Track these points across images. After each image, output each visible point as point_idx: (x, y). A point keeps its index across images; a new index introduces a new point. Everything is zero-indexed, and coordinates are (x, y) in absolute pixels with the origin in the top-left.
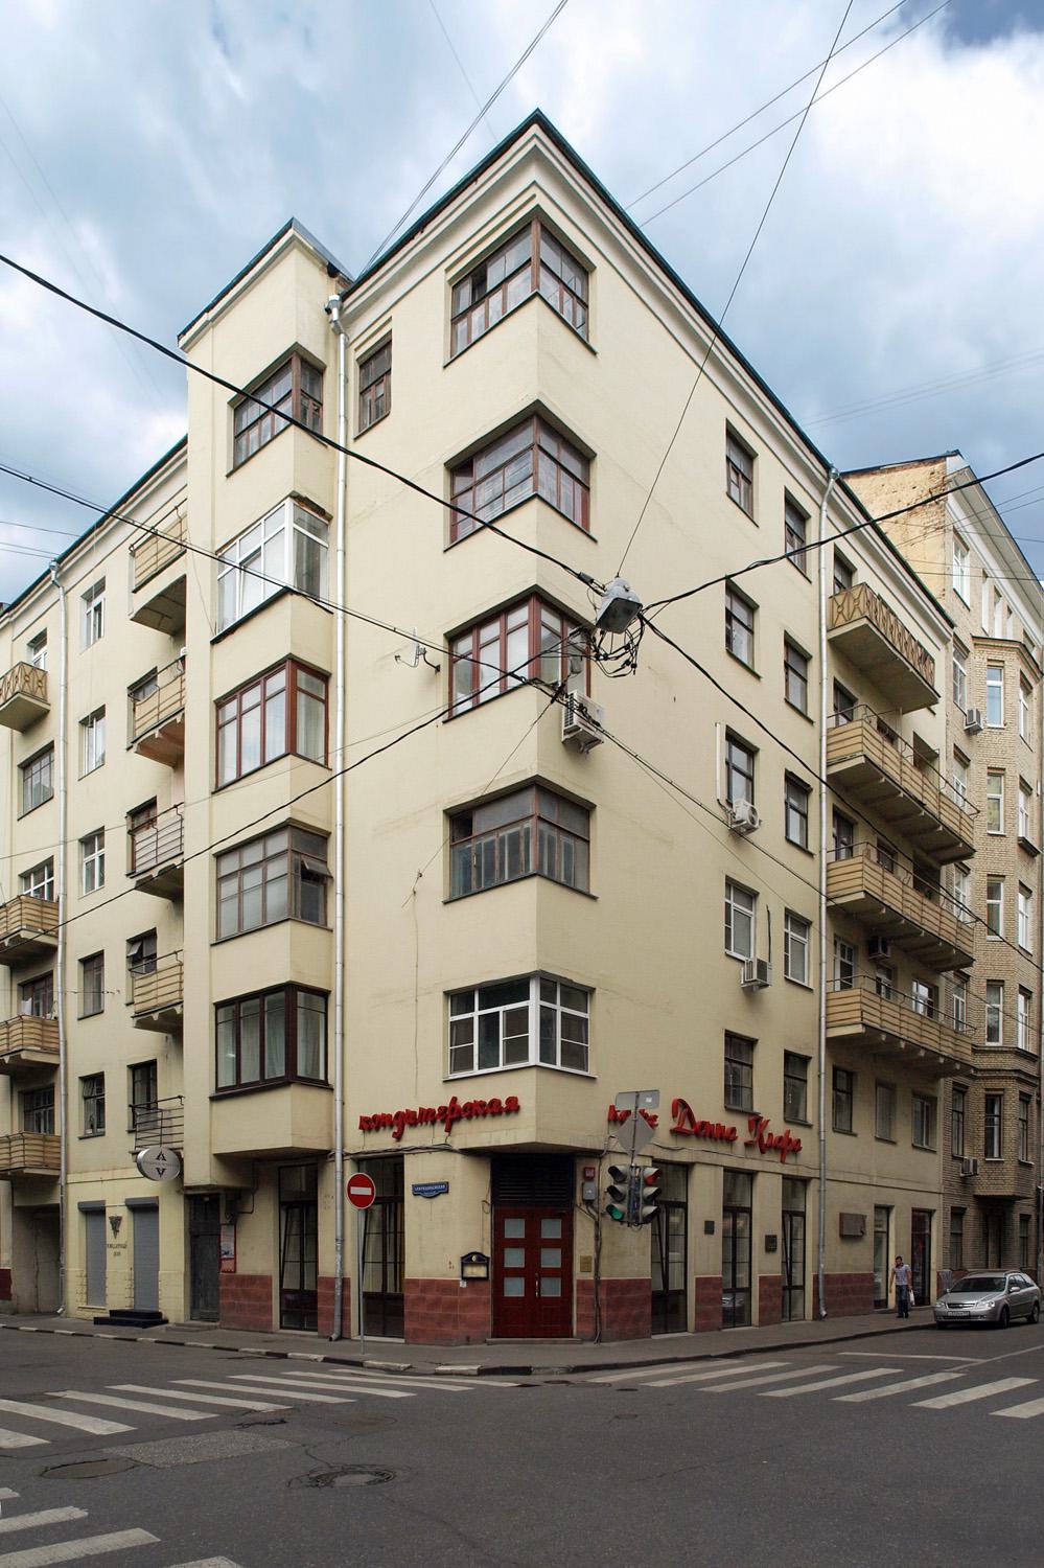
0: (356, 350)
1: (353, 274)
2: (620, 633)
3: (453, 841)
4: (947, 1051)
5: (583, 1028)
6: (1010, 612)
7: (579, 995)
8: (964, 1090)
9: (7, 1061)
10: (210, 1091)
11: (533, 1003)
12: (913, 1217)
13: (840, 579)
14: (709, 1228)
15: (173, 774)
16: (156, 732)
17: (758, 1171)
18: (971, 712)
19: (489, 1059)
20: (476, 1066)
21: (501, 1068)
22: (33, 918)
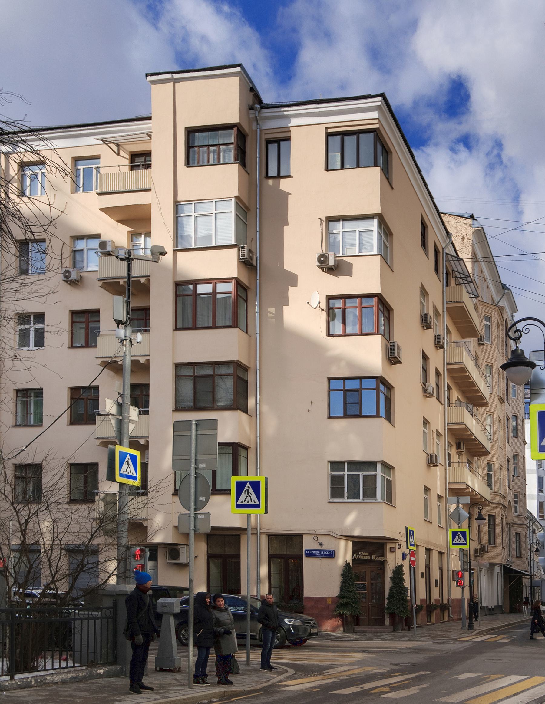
0: (319, 670)
1: (420, 152)
5: (399, 674)
6: (308, 303)
8: (41, 391)
9: (142, 282)
10: (382, 422)
13: (459, 397)
15: (115, 375)
20: (346, 498)
21: (360, 500)
22: (84, 649)
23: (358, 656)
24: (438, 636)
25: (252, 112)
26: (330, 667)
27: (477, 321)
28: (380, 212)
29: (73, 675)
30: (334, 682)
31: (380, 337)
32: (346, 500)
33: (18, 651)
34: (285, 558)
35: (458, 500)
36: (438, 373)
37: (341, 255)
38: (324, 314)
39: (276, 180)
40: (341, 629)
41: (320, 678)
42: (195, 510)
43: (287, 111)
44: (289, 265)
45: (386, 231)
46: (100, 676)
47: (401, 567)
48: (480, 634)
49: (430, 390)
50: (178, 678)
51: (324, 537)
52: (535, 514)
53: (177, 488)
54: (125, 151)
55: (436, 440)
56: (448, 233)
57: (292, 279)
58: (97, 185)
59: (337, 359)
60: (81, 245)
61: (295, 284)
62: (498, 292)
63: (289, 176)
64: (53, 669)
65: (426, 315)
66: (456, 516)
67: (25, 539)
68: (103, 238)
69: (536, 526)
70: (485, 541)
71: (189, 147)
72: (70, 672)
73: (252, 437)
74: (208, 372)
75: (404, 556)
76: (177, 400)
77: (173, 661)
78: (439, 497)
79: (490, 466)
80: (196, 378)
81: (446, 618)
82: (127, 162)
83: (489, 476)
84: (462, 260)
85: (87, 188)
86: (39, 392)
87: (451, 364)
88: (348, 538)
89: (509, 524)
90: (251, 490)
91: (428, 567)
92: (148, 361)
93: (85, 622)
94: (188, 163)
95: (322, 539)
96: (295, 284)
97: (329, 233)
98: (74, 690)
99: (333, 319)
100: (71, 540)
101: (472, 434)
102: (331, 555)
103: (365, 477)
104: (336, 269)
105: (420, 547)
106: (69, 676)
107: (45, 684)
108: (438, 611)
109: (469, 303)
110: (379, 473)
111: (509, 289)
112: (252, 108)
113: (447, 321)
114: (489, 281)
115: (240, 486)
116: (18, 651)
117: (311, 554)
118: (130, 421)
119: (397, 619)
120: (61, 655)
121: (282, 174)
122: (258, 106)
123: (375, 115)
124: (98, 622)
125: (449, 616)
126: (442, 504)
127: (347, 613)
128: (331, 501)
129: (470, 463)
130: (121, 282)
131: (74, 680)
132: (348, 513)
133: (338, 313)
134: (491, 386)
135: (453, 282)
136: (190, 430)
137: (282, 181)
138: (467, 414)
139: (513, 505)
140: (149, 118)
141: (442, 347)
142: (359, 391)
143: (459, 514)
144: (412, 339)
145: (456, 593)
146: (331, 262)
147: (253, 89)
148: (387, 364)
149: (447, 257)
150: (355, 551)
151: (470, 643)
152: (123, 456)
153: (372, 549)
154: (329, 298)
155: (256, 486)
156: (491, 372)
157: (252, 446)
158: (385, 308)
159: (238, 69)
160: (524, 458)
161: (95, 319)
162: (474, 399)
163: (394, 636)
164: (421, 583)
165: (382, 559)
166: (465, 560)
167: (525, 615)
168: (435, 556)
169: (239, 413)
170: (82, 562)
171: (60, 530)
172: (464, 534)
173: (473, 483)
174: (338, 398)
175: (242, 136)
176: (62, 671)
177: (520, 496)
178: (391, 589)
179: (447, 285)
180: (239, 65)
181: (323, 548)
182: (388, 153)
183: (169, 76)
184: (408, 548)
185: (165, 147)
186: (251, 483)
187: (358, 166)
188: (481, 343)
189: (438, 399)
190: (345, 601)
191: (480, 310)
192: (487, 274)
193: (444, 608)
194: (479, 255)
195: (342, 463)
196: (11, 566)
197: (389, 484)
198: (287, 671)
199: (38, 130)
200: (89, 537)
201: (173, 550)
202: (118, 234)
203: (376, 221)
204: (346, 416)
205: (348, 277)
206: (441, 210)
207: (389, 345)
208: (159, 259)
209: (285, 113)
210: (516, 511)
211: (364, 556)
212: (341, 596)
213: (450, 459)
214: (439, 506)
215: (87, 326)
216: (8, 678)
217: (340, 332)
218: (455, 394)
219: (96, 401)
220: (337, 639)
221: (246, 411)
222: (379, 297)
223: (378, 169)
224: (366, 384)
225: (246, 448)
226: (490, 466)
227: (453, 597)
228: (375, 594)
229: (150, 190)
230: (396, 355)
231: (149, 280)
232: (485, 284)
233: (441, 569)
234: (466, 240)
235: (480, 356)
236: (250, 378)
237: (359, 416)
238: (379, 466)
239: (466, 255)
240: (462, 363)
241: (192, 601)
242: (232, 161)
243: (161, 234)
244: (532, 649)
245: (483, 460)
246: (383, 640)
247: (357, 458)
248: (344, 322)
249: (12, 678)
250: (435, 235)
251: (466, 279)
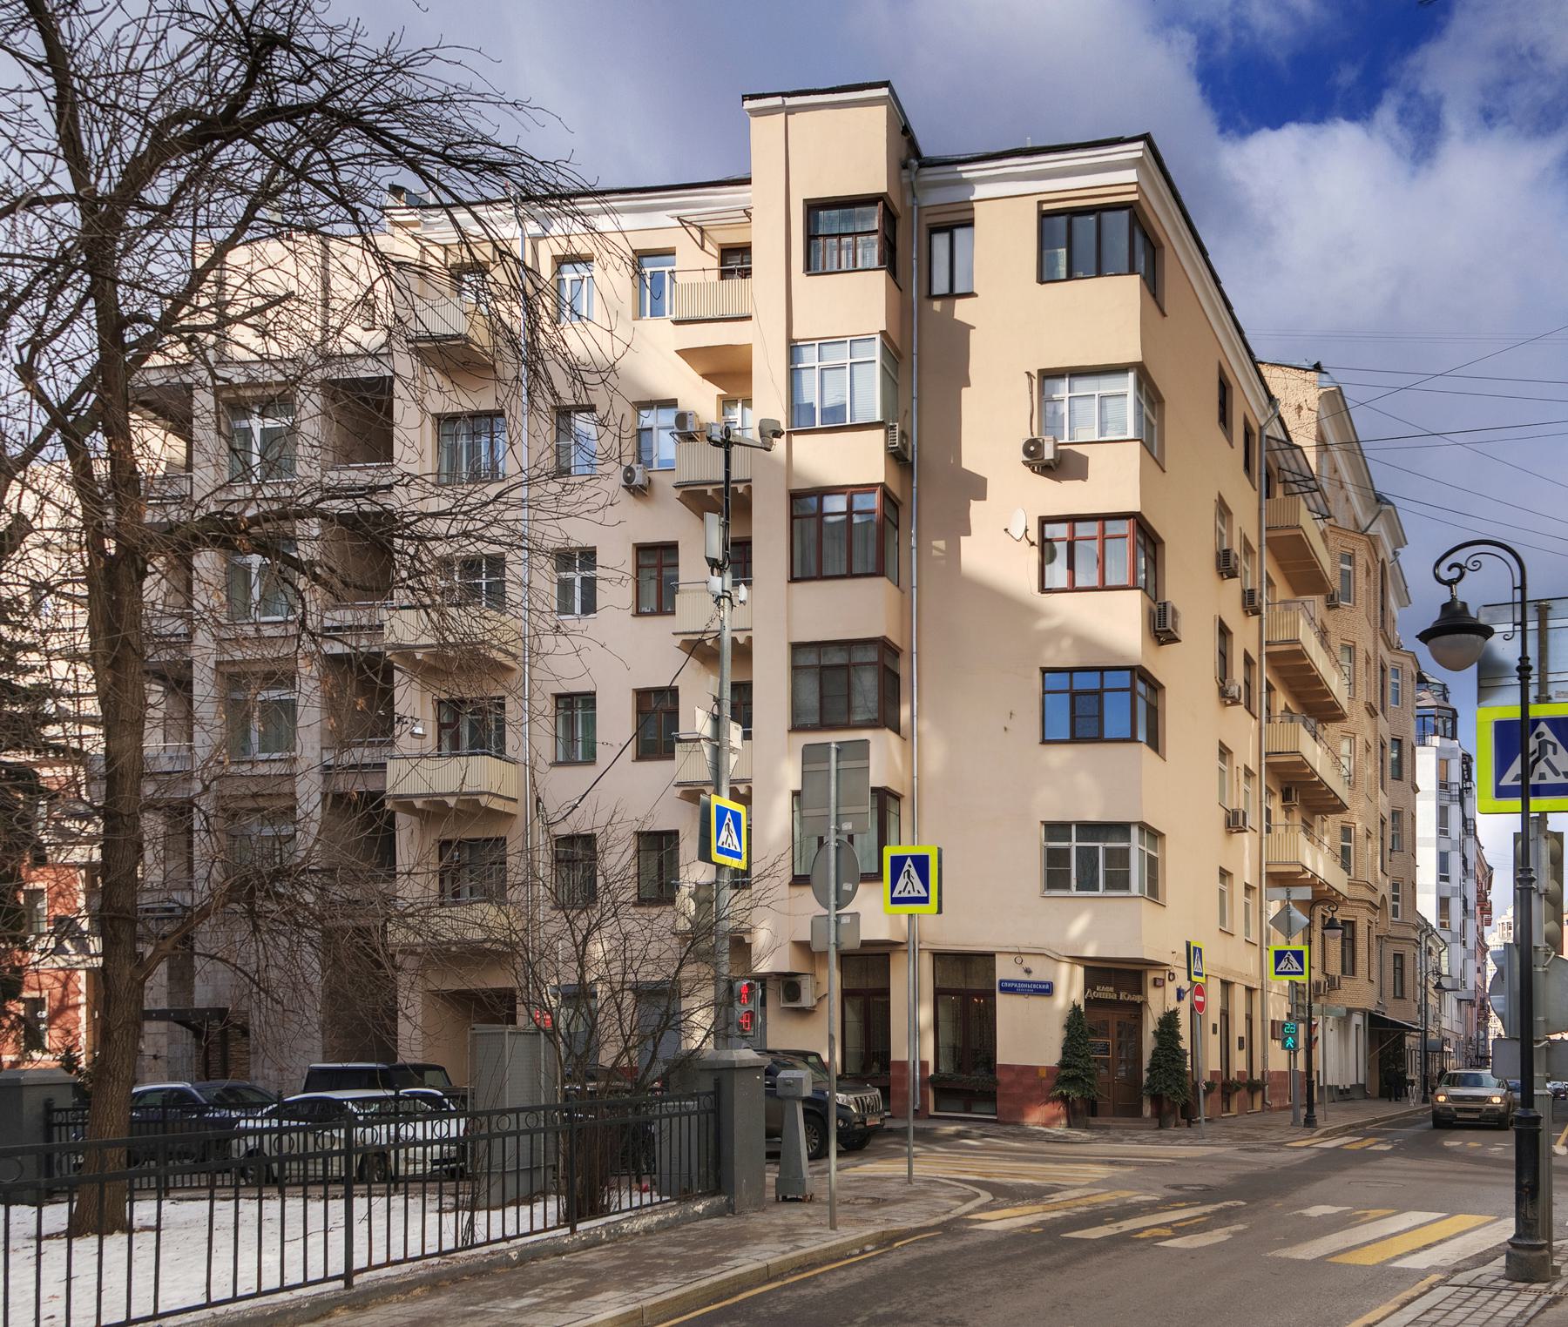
0: (1036, 1194)
2: (21, 379)
3: (344, 746)
4: (300, 450)
21: (1100, 893)
22: (675, 1169)
23: (1102, 1172)
24: (1245, 1137)
25: (905, 173)
26: (1054, 1189)
27: (1327, 562)
28: (1139, 359)
29: (661, 1217)
30: (1066, 1217)
31: (1138, 593)
32: (1074, 892)
33: (578, 1180)
34: (965, 995)
35: (1288, 893)
36: (1248, 661)
37: (1066, 440)
38: (1035, 551)
39: (947, 302)
40: (1064, 1122)
41: (1039, 1208)
42: (838, 907)
43: (969, 172)
44: (972, 458)
45: (1151, 395)
46: (698, 1217)
47: (1175, 1012)
48: (1327, 1135)
49: (1234, 691)
50: (811, 1212)
52: (1432, 919)
54: (712, 240)
55: (1243, 785)
56: (1271, 398)
57: (976, 487)
58: (676, 306)
59: (1058, 633)
60: (648, 419)
61: (981, 495)
62: (1367, 509)
63: (971, 295)
64: (631, 1209)
65: (1227, 553)
66: (1284, 923)
67: (583, 972)
68: (682, 407)
69: (1434, 942)
70: (1335, 968)
71: (811, 237)
72: (654, 1213)
73: (907, 778)
74: (837, 658)
75: (1180, 994)
76: (795, 712)
77: (802, 1183)
78: (1248, 888)
79: (1346, 832)
80: (823, 669)
81: (1258, 1105)
82: (715, 263)
83: (1345, 851)
84: (1300, 447)
85: (657, 312)
86: (589, 699)
87: (1275, 644)
88: (1077, 960)
91: (1225, 1015)
92: (750, 639)
93: (676, 1120)
94: (809, 268)
95: (1029, 962)
96: (981, 495)
97: (1044, 398)
98: (663, 1244)
99: (1052, 560)
100: (649, 974)
101: (1314, 773)
102: (1045, 990)
103: (1107, 850)
104: (1059, 465)
106: (655, 1218)
107: (621, 1236)
108: (1244, 1092)
109: (1312, 529)
110: (1136, 845)
111: (1389, 503)
112: (905, 166)
113: (1268, 565)
114: (1350, 487)
115: (898, 862)
116: (578, 1180)
117: (1011, 988)
118: (733, 750)
119: (1166, 1106)
120: (639, 1181)
121: (958, 290)
122: (914, 162)
123: (1131, 175)
124: (694, 1118)
125: (1264, 1102)
126: (1253, 901)
127: (1074, 1094)
128: (1047, 893)
129: (1308, 827)
130: (710, 490)
131: (664, 1226)
132: (1076, 915)
133: (1061, 548)
134: (1352, 684)
135: (1279, 492)
136: (828, 760)
137: (959, 303)
138: (1305, 736)
139: (1390, 903)
140: (747, 181)
141: (1257, 612)
142: (1099, 694)
143: (1289, 919)
144: (1200, 596)
145: (1277, 1059)
146: (1049, 454)
147: (906, 130)
148: (1151, 645)
149: (1268, 444)
150: (1089, 984)
151: (1307, 1152)
152: (722, 812)
153: (1117, 981)
154: (1044, 521)
155: (921, 863)
156: (1352, 659)
157: (907, 794)
158: (1148, 539)
159: (884, 92)
160: (1414, 817)
161: (672, 561)
162: (1317, 707)
163: (1160, 1136)
164: (1213, 1044)
165: (1138, 999)
166: (1301, 1001)
167: (1412, 1102)
168: (1239, 994)
169: (888, 734)
170: (667, 1011)
171: (635, 954)
172: (1298, 955)
173: (1315, 862)
174: (1061, 705)
175: (890, 218)
176: (644, 1211)
177: (1404, 888)
178: (1155, 1054)
179: (1268, 497)
180: (886, 84)
181: (1032, 978)
182: (1154, 249)
183: (777, 101)
184: (1189, 979)
185: (772, 237)
186: (913, 858)
187: (1099, 274)
188: (1332, 604)
189: (1248, 708)
190: (1071, 1072)
191: (1331, 544)
192: (1346, 474)
193: (1253, 1087)
194: (1331, 438)
195: (1067, 825)
196: (562, 1025)
197: (1153, 865)
198: (978, 1195)
199: (603, 193)
200: (677, 964)
201: (789, 984)
202: (702, 400)
203: (1131, 375)
204: (1074, 739)
205: (1080, 482)
206: (1258, 358)
207: (1155, 608)
208: (771, 443)
209: (965, 175)
210: (1395, 915)
211: (1106, 992)
212: (1063, 1065)
213: (1268, 819)
214: (1247, 904)
215: (660, 573)
216: (567, 1230)
217: (1064, 584)
218: (1281, 700)
219: (673, 715)
220: (1058, 1140)
221: (897, 730)
222: (1137, 519)
223: (1137, 278)
224: (1112, 680)
225: (898, 797)
226: (1346, 832)
227: (1271, 1069)
228: (1126, 1063)
229: (749, 318)
230: (1169, 626)
231: (749, 488)
232: (1342, 494)
233: (1249, 1018)
234: (1304, 412)
235: (1331, 627)
236: (903, 671)
237: (1099, 739)
238: (1135, 831)
239: (1305, 438)
240: (1297, 642)
242: (876, 265)
243: (768, 402)
245: (1333, 822)
246: (1140, 1142)
247: (1092, 817)
248: (1071, 566)
249: (573, 1231)
250: (1246, 402)
251: (1307, 483)
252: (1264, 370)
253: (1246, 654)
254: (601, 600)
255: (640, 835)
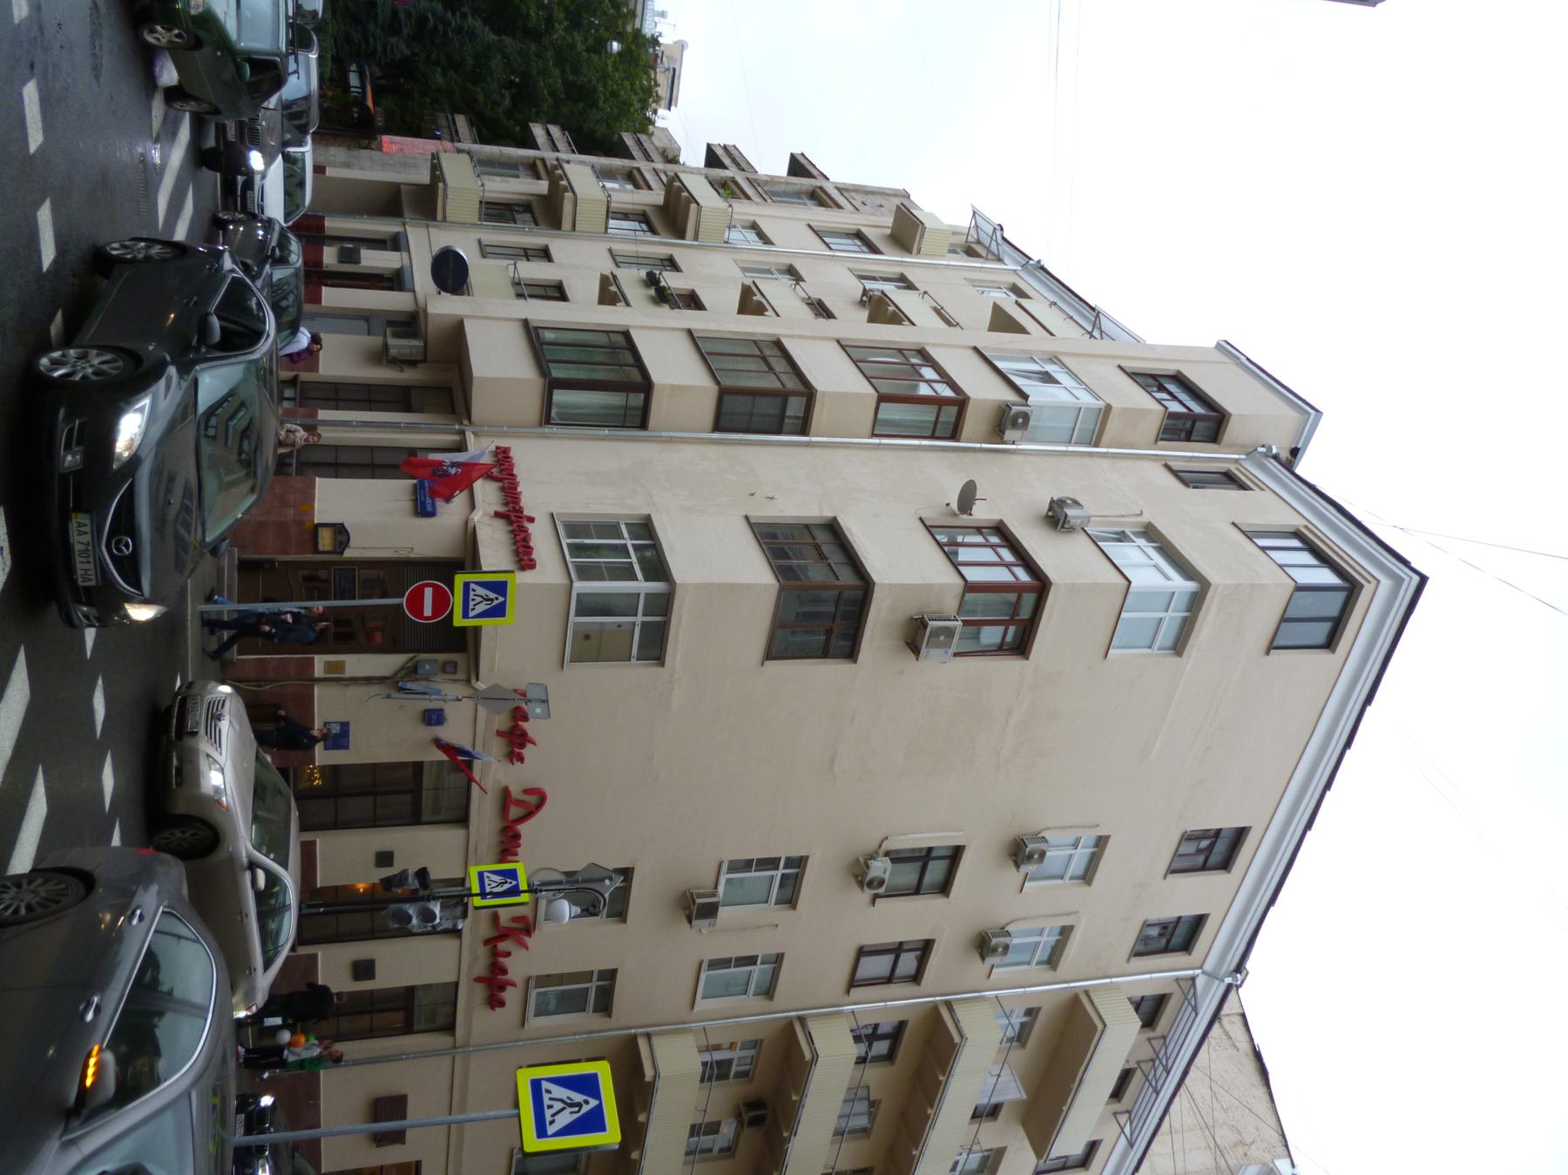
7: (655, 646)
11: (642, 586)
12: (409, 1164)
14: (385, 859)
16: (892, 308)
17: (467, 827)
18: (1008, 934)
19: (577, 550)
21: (565, 542)
51: (449, 1071)
53: (421, 455)
89: (1194, 984)
90: (506, 886)
95: (996, 559)
103: (577, 615)
105: (450, 943)
146: (284, 304)
198: (267, 965)
241: (612, 317)
244: (544, 436)
252: (962, 569)
253: (1028, 297)
254: (803, 272)
255: (648, 518)
